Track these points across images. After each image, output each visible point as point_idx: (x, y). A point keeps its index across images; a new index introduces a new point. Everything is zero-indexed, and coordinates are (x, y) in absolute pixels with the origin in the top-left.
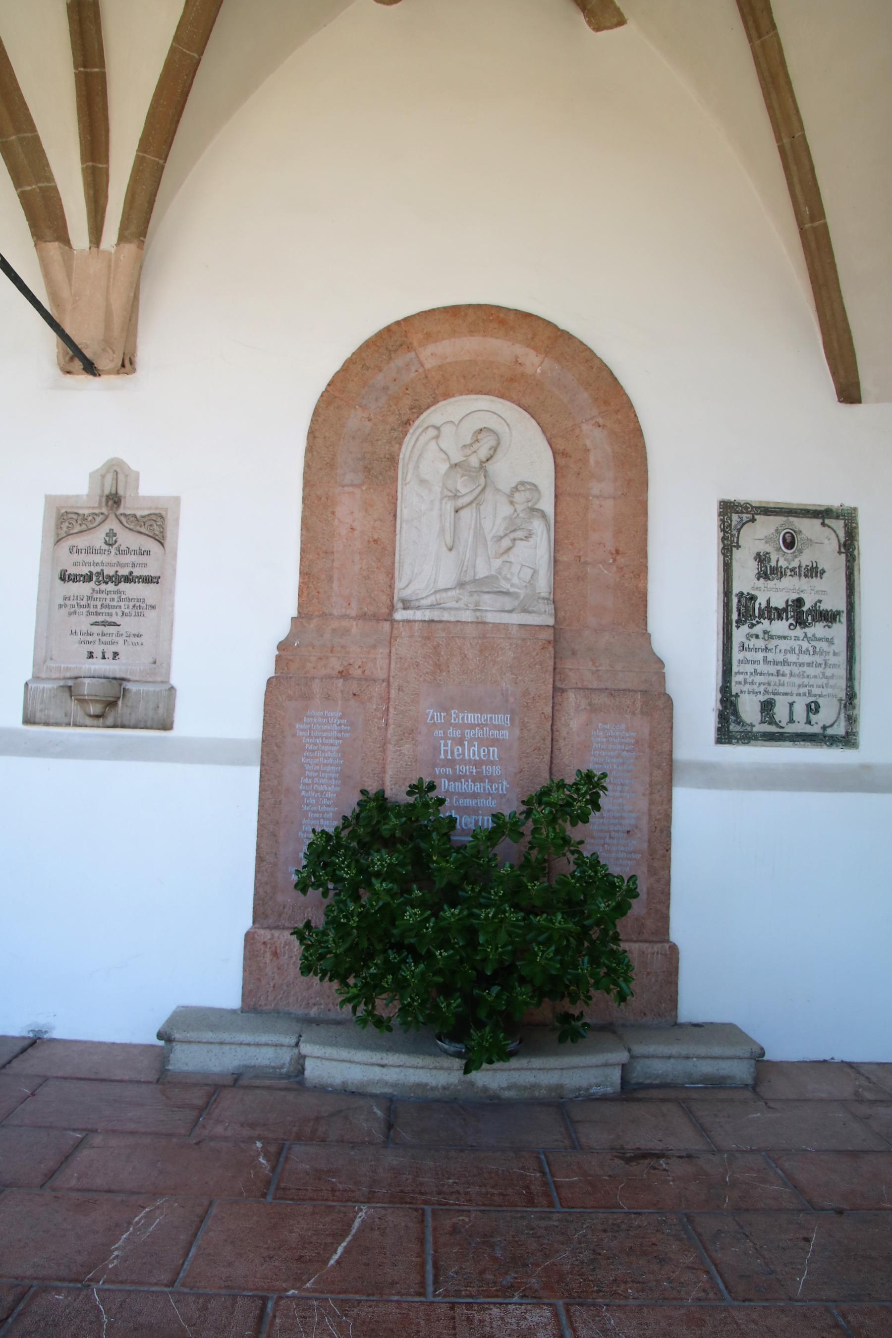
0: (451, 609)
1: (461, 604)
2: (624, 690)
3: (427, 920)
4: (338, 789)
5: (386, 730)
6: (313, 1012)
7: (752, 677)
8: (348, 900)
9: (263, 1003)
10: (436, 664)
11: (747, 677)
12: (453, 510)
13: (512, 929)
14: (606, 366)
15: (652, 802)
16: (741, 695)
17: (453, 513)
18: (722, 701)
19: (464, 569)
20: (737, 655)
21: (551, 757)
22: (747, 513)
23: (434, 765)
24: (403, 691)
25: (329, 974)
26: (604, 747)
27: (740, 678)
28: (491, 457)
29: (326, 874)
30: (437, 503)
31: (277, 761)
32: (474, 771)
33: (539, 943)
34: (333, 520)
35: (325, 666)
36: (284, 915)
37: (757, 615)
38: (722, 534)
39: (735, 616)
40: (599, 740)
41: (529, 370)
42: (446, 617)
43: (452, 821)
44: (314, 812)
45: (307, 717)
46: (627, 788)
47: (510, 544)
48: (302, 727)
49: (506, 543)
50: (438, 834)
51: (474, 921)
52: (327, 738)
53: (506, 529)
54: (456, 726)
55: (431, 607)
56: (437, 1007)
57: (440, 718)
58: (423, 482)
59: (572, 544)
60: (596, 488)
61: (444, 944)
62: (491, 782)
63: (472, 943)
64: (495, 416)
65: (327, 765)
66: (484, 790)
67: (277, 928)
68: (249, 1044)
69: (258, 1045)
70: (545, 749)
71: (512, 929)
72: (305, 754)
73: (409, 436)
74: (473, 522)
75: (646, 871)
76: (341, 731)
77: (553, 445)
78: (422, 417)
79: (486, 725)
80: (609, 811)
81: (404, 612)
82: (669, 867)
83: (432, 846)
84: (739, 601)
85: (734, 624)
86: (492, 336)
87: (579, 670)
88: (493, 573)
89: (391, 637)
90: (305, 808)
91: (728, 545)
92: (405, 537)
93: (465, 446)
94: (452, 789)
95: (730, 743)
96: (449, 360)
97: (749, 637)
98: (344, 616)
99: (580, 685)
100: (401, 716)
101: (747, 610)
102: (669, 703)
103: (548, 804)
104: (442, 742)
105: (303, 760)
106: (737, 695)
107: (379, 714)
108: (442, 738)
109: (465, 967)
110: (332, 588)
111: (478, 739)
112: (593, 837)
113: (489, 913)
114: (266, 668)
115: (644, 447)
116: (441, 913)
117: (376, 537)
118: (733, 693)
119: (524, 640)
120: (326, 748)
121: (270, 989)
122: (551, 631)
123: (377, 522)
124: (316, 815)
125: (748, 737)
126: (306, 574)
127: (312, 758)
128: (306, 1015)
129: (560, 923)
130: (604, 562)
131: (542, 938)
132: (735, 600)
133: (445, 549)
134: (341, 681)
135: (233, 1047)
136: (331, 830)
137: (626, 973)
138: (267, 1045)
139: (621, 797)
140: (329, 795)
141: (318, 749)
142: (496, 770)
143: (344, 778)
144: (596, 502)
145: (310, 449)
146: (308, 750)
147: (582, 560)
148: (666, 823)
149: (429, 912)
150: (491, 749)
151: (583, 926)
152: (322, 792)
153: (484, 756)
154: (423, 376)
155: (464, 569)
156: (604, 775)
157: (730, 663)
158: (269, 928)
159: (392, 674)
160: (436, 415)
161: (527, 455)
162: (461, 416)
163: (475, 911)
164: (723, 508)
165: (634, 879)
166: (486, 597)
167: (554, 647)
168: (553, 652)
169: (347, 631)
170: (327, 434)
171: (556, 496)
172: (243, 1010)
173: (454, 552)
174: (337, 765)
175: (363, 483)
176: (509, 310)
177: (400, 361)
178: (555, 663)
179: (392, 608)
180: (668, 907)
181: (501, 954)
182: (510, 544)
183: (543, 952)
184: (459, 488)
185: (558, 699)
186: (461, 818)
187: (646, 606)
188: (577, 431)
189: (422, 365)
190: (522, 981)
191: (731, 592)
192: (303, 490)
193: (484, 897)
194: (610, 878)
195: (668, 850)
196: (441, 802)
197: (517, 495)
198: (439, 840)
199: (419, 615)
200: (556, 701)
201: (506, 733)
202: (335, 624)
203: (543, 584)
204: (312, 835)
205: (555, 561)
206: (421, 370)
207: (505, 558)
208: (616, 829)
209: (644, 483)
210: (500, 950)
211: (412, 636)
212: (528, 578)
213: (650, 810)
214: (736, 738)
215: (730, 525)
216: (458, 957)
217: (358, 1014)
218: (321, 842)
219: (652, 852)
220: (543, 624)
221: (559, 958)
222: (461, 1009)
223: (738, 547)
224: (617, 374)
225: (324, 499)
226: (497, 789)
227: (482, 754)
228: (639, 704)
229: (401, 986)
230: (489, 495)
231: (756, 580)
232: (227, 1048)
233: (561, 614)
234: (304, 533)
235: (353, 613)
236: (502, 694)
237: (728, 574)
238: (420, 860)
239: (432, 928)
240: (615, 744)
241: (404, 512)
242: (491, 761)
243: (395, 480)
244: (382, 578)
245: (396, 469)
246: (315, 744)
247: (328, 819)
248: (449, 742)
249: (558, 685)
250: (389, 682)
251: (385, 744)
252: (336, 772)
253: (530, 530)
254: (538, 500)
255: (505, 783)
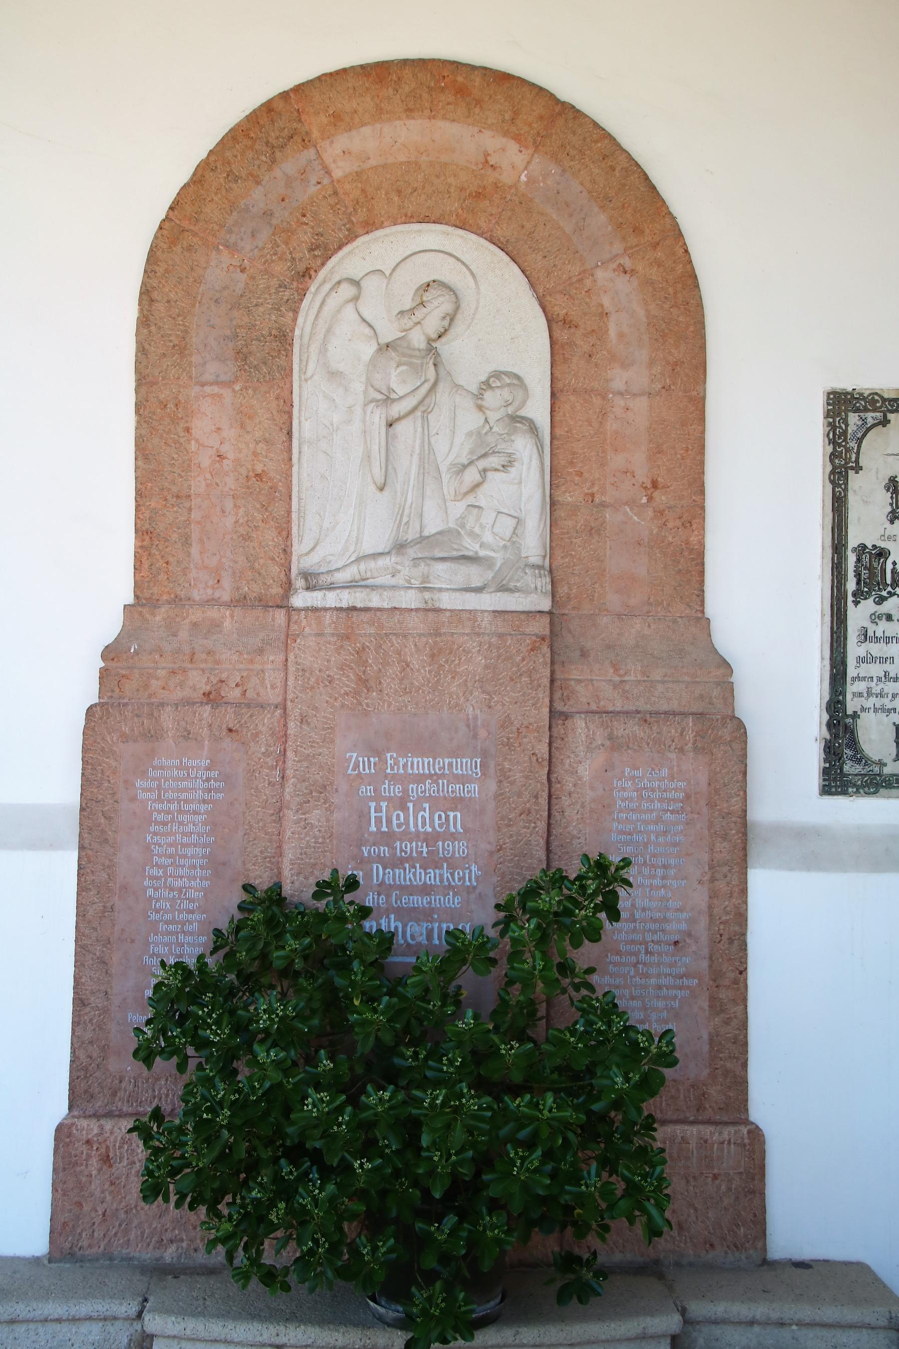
0: (382, 587)
1: (399, 580)
2: (665, 713)
3: (339, 1110)
4: (206, 883)
5: (282, 786)
6: (169, 1254)
7: (881, 685)
8: (217, 1079)
9: (85, 1243)
10: (360, 679)
11: (873, 684)
12: (384, 423)
13: (472, 1122)
14: (637, 165)
15: (714, 895)
16: (862, 715)
17: (384, 429)
18: (829, 725)
19: (405, 519)
20: (854, 650)
21: (549, 825)
22: (874, 411)
23: (361, 843)
24: (308, 724)
25: (189, 1199)
26: (634, 805)
27: (861, 686)
28: (446, 331)
29: (184, 1034)
30: (358, 409)
31: (106, 841)
32: (425, 850)
33: (518, 1144)
34: (189, 441)
35: (181, 685)
36: (121, 1094)
37: (889, 581)
38: (830, 449)
39: (851, 585)
40: (626, 794)
41: (507, 178)
42: (375, 601)
43: (386, 940)
44: (167, 923)
45: (154, 768)
46: (672, 872)
47: (478, 478)
48: (145, 784)
49: (471, 476)
50: (362, 962)
51: (414, 1111)
52: (186, 801)
53: (472, 452)
54: (394, 778)
55: (351, 585)
56: (355, 1252)
57: (367, 766)
58: (334, 375)
59: (580, 474)
60: (619, 378)
61: (369, 1148)
62: (452, 867)
63: (412, 1143)
64: (452, 260)
65: (187, 845)
66: (441, 881)
67: (109, 1115)
68: (59, 1320)
69: (74, 1320)
70: (537, 812)
71: (472, 1122)
72: (152, 829)
73: (309, 296)
74: (418, 442)
75: (706, 1005)
76: (209, 791)
77: (548, 308)
78: (330, 264)
79: (443, 776)
80: (644, 910)
81: (308, 594)
82: (745, 1000)
83: (353, 984)
84: (859, 560)
85: (850, 598)
86: (444, 118)
87: (592, 682)
88: (452, 525)
89: (287, 636)
90: (153, 916)
91: (841, 466)
92: (308, 471)
93: (401, 313)
94: (389, 881)
95: (844, 793)
96: (373, 162)
97: (875, 618)
98: (211, 602)
99: (594, 707)
100: (305, 764)
101: (872, 575)
102: (740, 732)
103: (536, 913)
104: (373, 805)
105: (149, 838)
106: (855, 715)
107: (270, 761)
108: (371, 799)
109: (402, 1184)
110: (189, 555)
111: (430, 799)
112: (619, 953)
113: (436, 1098)
114: (87, 691)
115: (700, 305)
116: (363, 1098)
117: (259, 468)
118: (849, 712)
119: (501, 636)
120: (185, 818)
121: (98, 1220)
122: (546, 620)
123: (260, 445)
124: (171, 927)
125: (875, 783)
126: (146, 533)
127: (162, 835)
128: (157, 1260)
129: (550, 1111)
130: (632, 503)
131: (523, 1134)
132: (852, 559)
133: (372, 488)
134: (208, 708)
135: (32, 1326)
136: (191, 962)
137: (659, 1189)
138: (90, 1318)
139: (664, 886)
140: (193, 894)
141: (173, 820)
142: (459, 848)
143: (216, 865)
144: (620, 402)
145: (144, 322)
146: (157, 823)
147: (597, 500)
148: (737, 928)
149: (344, 1097)
150: (451, 814)
151: (589, 1113)
152: (180, 890)
153: (440, 826)
154: (330, 192)
155: (405, 519)
156: (626, 862)
157: (844, 663)
158: (96, 1116)
159: (290, 696)
160: (353, 260)
161: (504, 327)
162: (393, 260)
163: (417, 1093)
164: (833, 404)
165: (667, 1038)
166: (440, 567)
167: (551, 647)
168: (548, 655)
169: (216, 626)
170: (172, 295)
171: (553, 395)
172: (51, 1258)
173: (386, 493)
174: (205, 846)
175: (236, 380)
176: (473, 68)
177: (290, 164)
178: (553, 672)
179: (288, 587)
180: (745, 1065)
181: (454, 1165)
182: (478, 478)
183: (523, 1159)
184: (394, 386)
185: (559, 730)
186: (405, 926)
187: (702, 573)
188: (588, 282)
189: (328, 173)
190: (494, 1205)
191: (845, 546)
192: (137, 392)
193: (430, 1068)
194: (632, 1034)
195: (743, 972)
196: (365, 912)
197: (488, 395)
198: (363, 974)
199: (331, 599)
200: (555, 734)
201: (474, 787)
202: (196, 615)
203: (533, 543)
204: (160, 972)
205: (553, 503)
206: (326, 181)
207: (470, 499)
208: (655, 938)
209: (701, 367)
210: (454, 1158)
211: (320, 634)
212: (508, 534)
213: (710, 907)
214: (854, 785)
215: (845, 432)
216: (389, 1171)
217: (237, 1262)
218: (175, 982)
219: (716, 975)
220: (533, 609)
221: (549, 1167)
222: (394, 1256)
223: (858, 468)
224: (656, 177)
225: (171, 405)
226: (462, 879)
227: (437, 822)
228: (690, 736)
229: (300, 1219)
230: (443, 395)
231: (887, 524)
232: (21, 1329)
233: (563, 590)
234: (140, 463)
235: (226, 597)
236: (468, 726)
237: (840, 516)
238: (334, 1003)
239: (348, 1124)
240: (652, 801)
241: (305, 426)
242: (452, 834)
243: (288, 373)
244: (270, 536)
245: (289, 354)
246: (168, 812)
247: (191, 934)
248: (384, 805)
249: (559, 706)
250: (285, 709)
251: (281, 809)
252: (203, 857)
253: (510, 455)
254: (524, 402)
255: (474, 868)
